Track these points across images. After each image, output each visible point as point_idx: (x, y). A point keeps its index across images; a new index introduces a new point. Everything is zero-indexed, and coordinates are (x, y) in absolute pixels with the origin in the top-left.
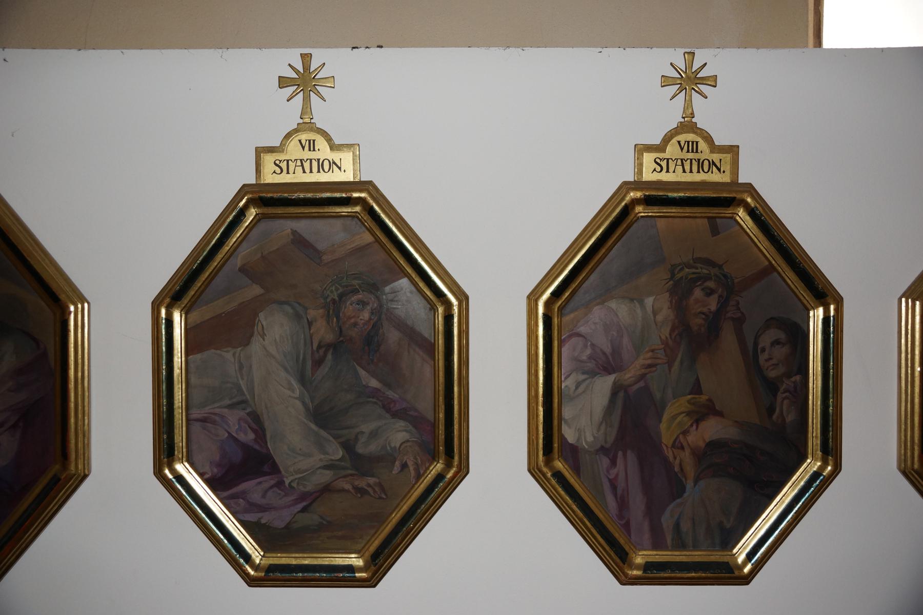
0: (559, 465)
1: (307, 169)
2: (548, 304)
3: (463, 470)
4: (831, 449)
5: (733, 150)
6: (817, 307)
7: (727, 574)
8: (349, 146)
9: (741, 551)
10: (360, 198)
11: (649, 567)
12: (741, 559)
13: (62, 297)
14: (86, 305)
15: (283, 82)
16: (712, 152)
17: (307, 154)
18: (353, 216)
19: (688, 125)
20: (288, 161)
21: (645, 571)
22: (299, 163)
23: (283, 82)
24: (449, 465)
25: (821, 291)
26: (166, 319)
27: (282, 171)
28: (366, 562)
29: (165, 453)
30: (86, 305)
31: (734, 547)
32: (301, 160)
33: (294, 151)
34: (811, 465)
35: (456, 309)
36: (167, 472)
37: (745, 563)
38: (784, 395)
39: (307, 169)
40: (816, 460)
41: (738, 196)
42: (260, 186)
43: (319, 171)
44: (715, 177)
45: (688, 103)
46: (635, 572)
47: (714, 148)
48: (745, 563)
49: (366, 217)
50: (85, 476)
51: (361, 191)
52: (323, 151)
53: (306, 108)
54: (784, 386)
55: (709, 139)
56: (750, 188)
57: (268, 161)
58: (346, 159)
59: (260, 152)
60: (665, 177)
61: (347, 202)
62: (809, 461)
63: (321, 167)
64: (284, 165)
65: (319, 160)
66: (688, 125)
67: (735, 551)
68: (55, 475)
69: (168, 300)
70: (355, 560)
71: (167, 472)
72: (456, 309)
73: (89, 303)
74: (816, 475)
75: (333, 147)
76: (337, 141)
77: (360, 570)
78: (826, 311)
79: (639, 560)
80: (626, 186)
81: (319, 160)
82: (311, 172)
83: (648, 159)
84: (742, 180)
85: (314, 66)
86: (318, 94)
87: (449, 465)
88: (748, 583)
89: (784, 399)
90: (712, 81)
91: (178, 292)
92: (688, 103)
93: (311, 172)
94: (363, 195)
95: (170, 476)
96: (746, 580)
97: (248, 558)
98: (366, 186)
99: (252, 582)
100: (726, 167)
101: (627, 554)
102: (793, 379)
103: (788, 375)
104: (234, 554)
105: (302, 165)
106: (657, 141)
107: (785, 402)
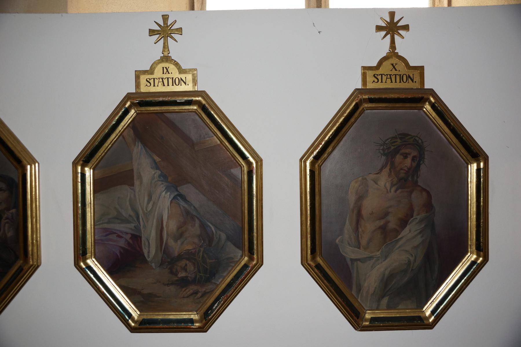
0: (319, 260)
1: (166, 84)
2: (312, 164)
3: (260, 263)
4: (482, 248)
5: (421, 69)
6: (473, 163)
7: (419, 323)
8: (191, 70)
9: (428, 310)
10: (197, 101)
11: (373, 320)
12: (428, 313)
13: (25, 162)
14: (37, 165)
15: (152, 32)
16: (180, 73)
17: (165, 76)
18: (195, 112)
19: (393, 53)
20: (154, 79)
21: (370, 322)
22: (389, 76)
23: (152, 32)
24: (251, 259)
25: (475, 153)
26: (81, 173)
27: (378, 82)
28: (201, 317)
29: (80, 253)
30: (37, 165)
31: (423, 307)
32: (162, 79)
33: (158, 73)
34: (471, 257)
35: (254, 165)
36: (82, 264)
37: (430, 316)
38: (6, 221)
39: (166, 84)
40: (473, 254)
41: (425, 97)
42: (138, 94)
43: (173, 85)
44: (410, 85)
45: (393, 42)
46: (367, 323)
47: (181, 71)
48: (430, 316)
49: (200, 111)
50: (38, 267)
51: (198, 96)
52: (175, 73)
53: (166, 47)
54: (6, 216)
55: (177, 64)
56: (432, 92)
57: (143, 79)
58: (189, 77)
59: (138, 75)
60: (152, 89)
61: (189, 103)
62: (469, 254)
63: (174, 82)
64: (379, 77)
65: (400, 75)
66: (393, 53)
67: (424, 309)
68: (20, 266)
69: (81, 162)
70: (194, 316)
71: (82, 264)
72: (254, 165)
73: (38, 164)
74: (473, 263)
75: (181, 71)
76: (148, 68)
77: (197, 321)
78: (479, 165)
79: (368, 316)
80: (129, 96)
81: (173, 78)
82: (168, 85)
83: (370, 73)
84: (426, 87)
85: (170, 22)
86: (172, 38)
87: (251, 259)
88: (73, 163)
89: (6, 223)
90: (180, 31)
91: (86, 158)
92: (393, 42)
93: (168, 85)
94: (200, 98)
95: (84, 267)
96: (431, 326)
97: (130, 315)
98: (203, 94)
99: (133, 330)
100: (417, 78)
101: (359, 313)
102: (11, 211)
103: (8, 209)
104: (122, 314)
105: (391, 78)
106: (375, 64)
107: (7, 225)
